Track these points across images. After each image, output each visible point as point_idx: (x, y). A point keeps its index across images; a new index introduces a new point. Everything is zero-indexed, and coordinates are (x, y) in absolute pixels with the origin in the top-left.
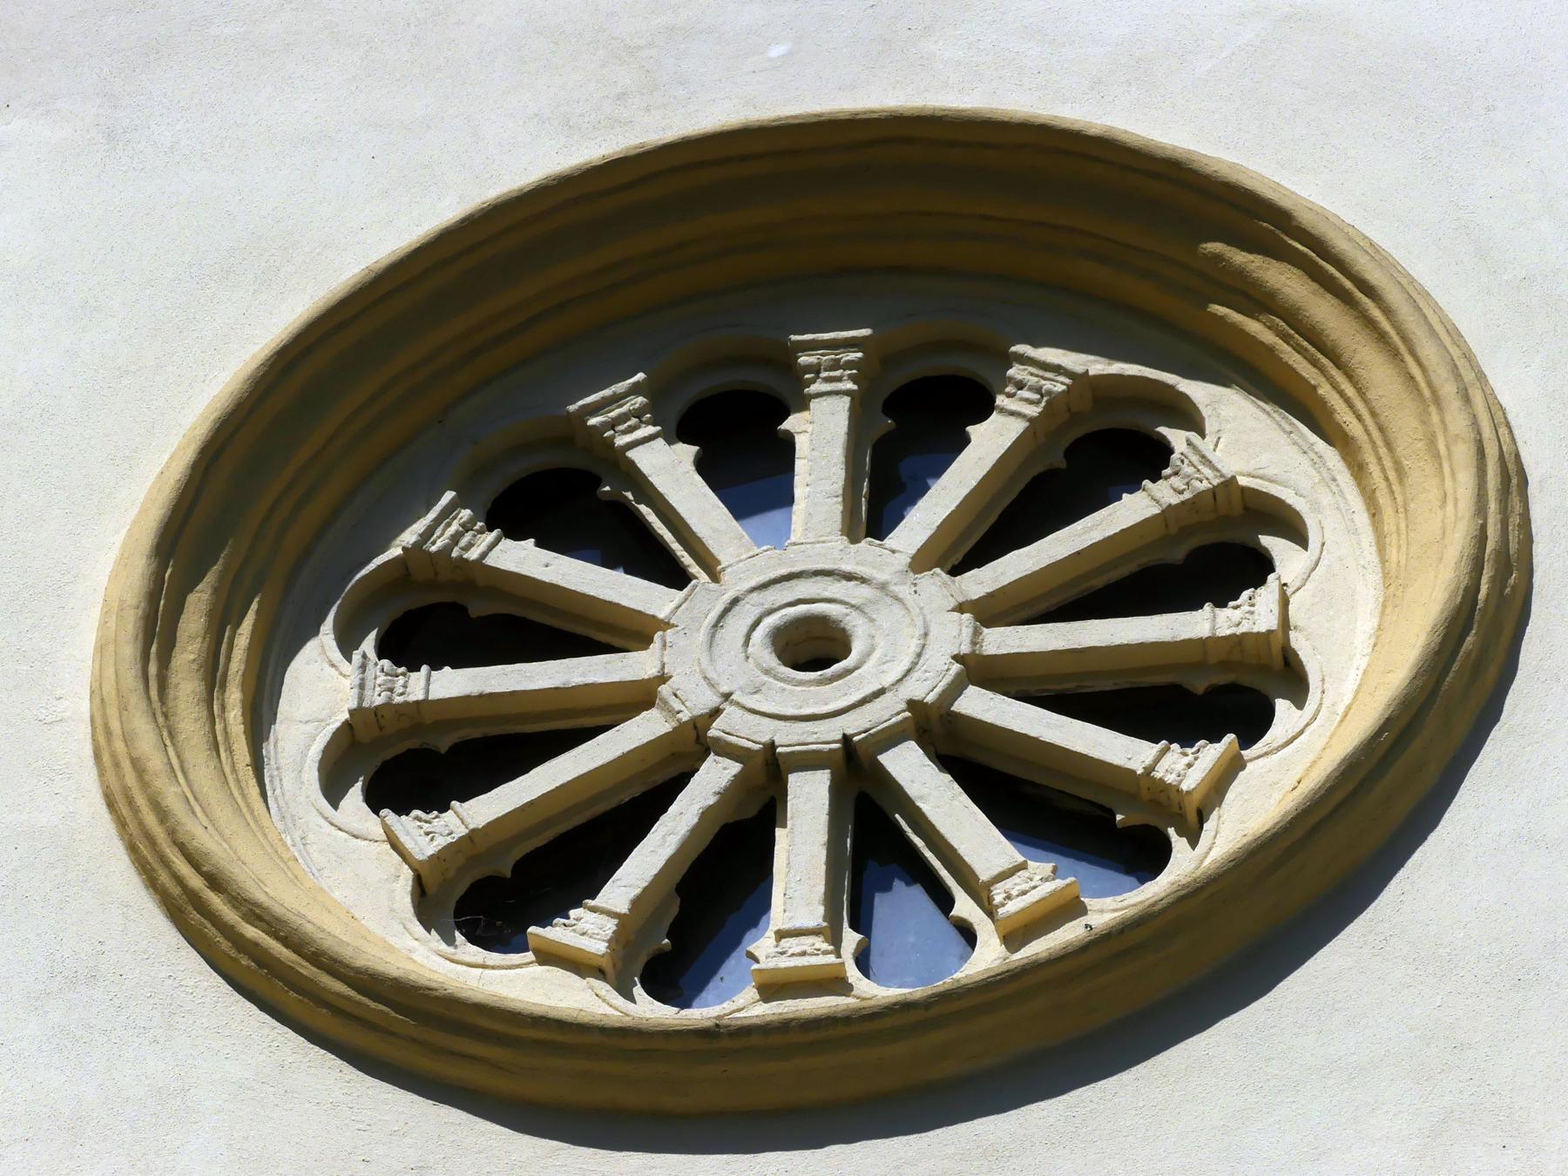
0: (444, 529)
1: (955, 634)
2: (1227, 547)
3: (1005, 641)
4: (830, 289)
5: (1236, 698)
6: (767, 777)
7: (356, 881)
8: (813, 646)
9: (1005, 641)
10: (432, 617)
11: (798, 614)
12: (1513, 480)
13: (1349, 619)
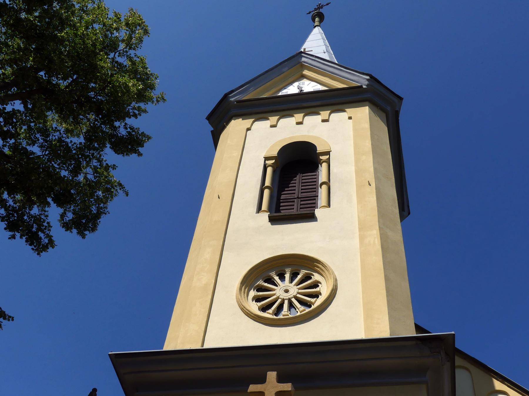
0: (261, 282)
1: (297, 290)
2: (316, 285)
3: (300, 291)
4: (288, 266)
5: (316, 295)
6: (283, 300)
7: (254, 307)
8: (287, 291)
9: (300, 291)
10: (260, 289)
11: (286, 289)
12: (336, 280)
13: (325, 290)
